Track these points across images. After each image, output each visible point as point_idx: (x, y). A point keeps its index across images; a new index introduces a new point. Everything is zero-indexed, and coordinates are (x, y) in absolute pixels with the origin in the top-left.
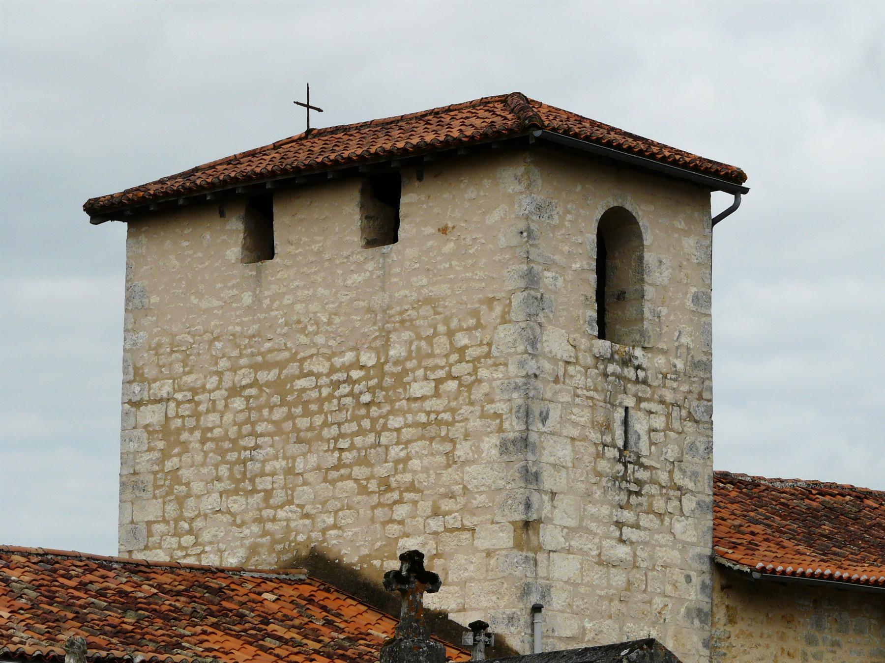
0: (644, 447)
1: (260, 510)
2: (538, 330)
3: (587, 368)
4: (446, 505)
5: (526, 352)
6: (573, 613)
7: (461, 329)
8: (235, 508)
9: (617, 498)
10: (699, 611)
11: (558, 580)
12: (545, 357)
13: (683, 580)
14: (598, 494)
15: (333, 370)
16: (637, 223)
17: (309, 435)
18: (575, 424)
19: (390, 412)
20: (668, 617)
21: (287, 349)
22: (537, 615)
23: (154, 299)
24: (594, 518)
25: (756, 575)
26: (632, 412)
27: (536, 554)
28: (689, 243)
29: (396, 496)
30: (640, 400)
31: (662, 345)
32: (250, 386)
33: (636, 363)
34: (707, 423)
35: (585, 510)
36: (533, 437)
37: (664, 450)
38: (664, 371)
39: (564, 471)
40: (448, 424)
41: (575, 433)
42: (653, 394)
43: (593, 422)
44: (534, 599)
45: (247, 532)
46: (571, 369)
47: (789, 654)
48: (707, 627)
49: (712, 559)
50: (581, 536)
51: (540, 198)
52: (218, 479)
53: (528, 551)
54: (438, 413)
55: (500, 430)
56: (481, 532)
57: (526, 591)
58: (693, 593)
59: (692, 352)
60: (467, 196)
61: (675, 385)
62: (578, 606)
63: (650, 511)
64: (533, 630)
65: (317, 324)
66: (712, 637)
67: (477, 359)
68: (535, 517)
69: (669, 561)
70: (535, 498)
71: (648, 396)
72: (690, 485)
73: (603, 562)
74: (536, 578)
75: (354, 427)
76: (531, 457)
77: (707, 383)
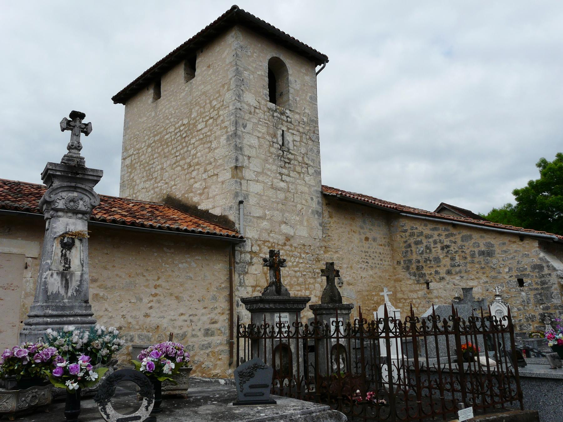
0: (291, 146)
1: (154, 185)
2: (241, 92)
3: (265, 112)
4: (209, 167)
5: (236, 99)
6: (260, 207)
7: (214, 99)
8: (147, 186)
9: (279, 163)
10: (317, 212)
11: (252, 192)
12: (245, 103)
13: (310, 199)
14: (271, 161)
15: (176, 129)
16: (286, 66)
17: (168, 154)
18: (259, 132)
19: (191, 138)
20: (304, 213)
21: (163, 126)
22: (241, 205)
23: (131, 123)
24: (269, 170)
25: (338, 196)
26: (285, 132)
27: (241, 180)
28: (307, 78)
29: (193, 168)
30: (289, 129)
31: (297, 111)
32: (153, 143)
33: (287, 115)
34: (317, 142)
35: (265, 166)
36: (239, 133)
37: (300, 149)
38: (299, 120)
39: (254, 149)
40: (209, 136)
41: (260, 135)
42: (294, 128)
43: (268, 133)
44: (240, 199)
45: (150, 193)
46: (257, 111)
47: (354, 232)
48: (321, 218)
49: (322, 192)
50: (263, 176)
51: (242, 44)
52: (143, 177)
53: (237, 178)
54: (206, 133)
55: (227, 132)
56: (220, 175)
57: (236, 195)
58: (314, 204)
59: (310, 116)
60: (216, 51)
61: (304, 126)
62: (262, 204)
63: (294, 170)
64: (239, 212)
65: (172, 115)
66: (323, 222)
67: (219, 108)
68: (240, 165)
69: (303, 191)
70: (240, 157)
71: (292, 128)
72: (312, 164)
73: (272, 187)
74: (241, 190)
75: (181, 147)
76: (238, 141)
77: (316, 128)
